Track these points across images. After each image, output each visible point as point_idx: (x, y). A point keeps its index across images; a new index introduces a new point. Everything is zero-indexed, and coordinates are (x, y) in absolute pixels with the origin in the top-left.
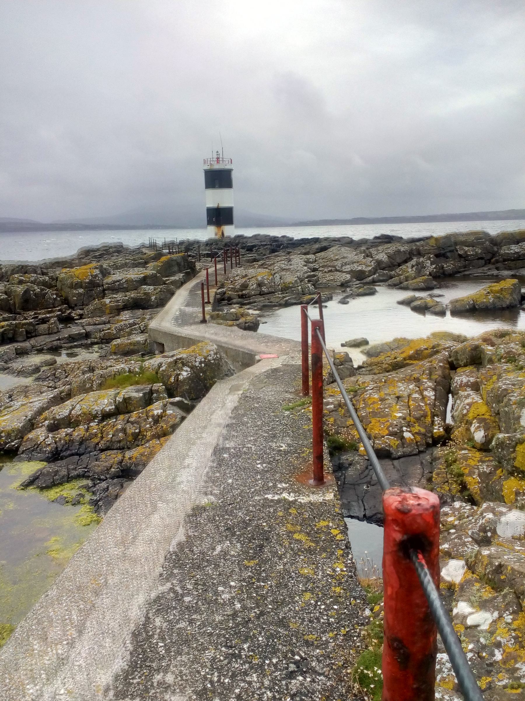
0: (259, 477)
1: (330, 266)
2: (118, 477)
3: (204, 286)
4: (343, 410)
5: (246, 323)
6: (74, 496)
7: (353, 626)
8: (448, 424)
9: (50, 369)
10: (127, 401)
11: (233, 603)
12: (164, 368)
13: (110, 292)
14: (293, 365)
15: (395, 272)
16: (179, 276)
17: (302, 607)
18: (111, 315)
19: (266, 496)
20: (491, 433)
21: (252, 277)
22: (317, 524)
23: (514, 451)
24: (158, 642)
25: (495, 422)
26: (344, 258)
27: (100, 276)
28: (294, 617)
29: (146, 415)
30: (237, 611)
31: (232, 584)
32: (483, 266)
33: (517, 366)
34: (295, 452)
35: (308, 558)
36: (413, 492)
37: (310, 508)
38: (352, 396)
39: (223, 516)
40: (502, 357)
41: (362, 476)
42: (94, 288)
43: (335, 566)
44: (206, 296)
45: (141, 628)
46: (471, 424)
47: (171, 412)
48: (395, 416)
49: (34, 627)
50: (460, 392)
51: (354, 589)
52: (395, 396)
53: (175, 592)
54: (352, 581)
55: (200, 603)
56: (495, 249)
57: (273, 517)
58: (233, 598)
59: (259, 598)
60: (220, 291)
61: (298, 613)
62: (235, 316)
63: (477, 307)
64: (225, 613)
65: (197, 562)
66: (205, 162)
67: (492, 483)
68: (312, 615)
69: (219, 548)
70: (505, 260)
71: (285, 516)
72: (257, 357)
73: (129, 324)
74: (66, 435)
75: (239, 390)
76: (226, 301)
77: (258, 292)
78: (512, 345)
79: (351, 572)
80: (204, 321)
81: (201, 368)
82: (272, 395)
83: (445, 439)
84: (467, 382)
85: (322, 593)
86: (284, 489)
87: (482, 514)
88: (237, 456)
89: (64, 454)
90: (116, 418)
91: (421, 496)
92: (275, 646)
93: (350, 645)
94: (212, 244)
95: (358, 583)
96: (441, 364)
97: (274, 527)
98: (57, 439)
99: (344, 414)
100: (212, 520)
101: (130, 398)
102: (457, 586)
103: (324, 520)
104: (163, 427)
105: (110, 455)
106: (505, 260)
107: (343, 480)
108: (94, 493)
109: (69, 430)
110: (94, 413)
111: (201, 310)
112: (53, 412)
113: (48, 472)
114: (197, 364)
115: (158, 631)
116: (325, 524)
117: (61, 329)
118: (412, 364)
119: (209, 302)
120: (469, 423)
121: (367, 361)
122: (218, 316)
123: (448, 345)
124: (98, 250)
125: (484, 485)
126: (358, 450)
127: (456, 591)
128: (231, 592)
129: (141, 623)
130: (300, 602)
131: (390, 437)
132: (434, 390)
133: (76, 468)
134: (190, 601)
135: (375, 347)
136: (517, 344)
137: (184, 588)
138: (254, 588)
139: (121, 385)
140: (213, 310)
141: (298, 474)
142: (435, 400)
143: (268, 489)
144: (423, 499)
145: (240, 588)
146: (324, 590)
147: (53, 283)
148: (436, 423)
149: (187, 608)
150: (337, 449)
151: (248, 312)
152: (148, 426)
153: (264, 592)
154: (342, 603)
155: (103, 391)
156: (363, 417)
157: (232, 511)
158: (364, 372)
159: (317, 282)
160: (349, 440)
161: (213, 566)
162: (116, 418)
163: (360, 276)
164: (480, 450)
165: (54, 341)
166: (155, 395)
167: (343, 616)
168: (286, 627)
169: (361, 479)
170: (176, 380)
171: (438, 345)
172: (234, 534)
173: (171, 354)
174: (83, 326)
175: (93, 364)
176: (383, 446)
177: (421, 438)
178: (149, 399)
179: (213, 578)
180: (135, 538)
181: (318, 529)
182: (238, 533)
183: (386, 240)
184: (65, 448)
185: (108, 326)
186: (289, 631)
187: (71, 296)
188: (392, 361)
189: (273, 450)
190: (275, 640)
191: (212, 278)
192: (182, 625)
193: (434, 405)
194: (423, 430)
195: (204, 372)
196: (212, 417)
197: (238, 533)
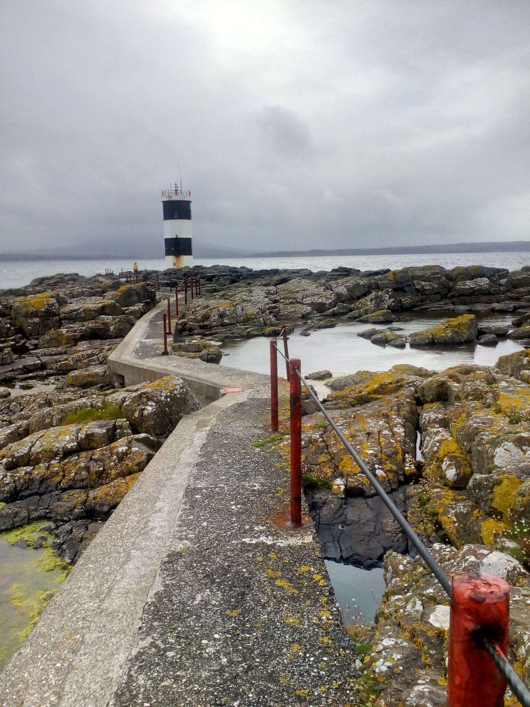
0: (234, 519)
1: (291, 298)
2: (82, 518)
3: (166, 316)
4: (314, 447)
5: (208, 355)
6: (36, 539)
7: (345, 678)
8: (419, 461)
9: (4, 402)
10: (90, 437)
11: (219, 657)
12: (128, 403)
13: (67, 321)
14: (259, 399)
15: (355, 305)
16: (138, 307)
17: (290, 660)
18: (68, 345)
19: (243, 540)
20: (462, 471)
21: (214, 308)
22: (298, 569)
23: (492, 492)
24: (143, 703)
25: (466, 460)
26: (304, 290)
27: (57, 305)
28: (284, 671)
29: (111, 453)
30: (223, 666)
31: (216, 636)
32: (439, 301)
33: (484, 404)
34: (269, 492)
35: (292, 607)
36: (482, 578)
37: (290, 552)
38: (322, 432)
39: (200, 562)
40: (468, 395)
41: (337, 516)
42: (50, 318)
43: (321, 614)
44: (167, 326)
45: (124, 687)
46: (442, 461)
47: (137, 449)
48: (367, 453)
49: (7, 690)
50: (428, 428)
51: (342, 639)
52: (365, 432)
53: (156, 647)
54: (339, 630)
55: (183, 658)
56: (451, 284)
57: (253, 562)
58: (218, 651)
59: (245, 651)
60: (181, 321)
61: (287, 667)
62: (197, 347)
63: (436, 341)
64: (212, 668)
65: (177, 613)
66: (163, 194)
67: (470, 523)
68: (302, 668)
69: (199, 598)
70: (460, 295)
71: (265, 561)
72: (222, 391)
73: (87, 355)
74: (26, 474)
75: (206, 426)
76: (187, 332)
77: (220, 324)
78: (478, 382)
79: (337, 620)
80: (165, 353)
81: (167, 402)
82: (240, 431)
83: (417, 476)
84: (435, 419)
85: (310, 644)
86: (261, 532)
87: (464, 557)
88: (210, 496)
89: (24, 493)
90: (78, 456)
91: (491, 582)
92: (266, 702)
93: (344, 700)
94: (171, 273)
95: (345, 632)
96: (408, 400)
97: (255, 573)
98: (16, 478)
99: (315, 451)
100: (189, 567)
101: (92, 434)
102: (446, 634)
103: (305, 565)
104: (128, 465)
105: (72, 495)
106: (460, 295)
107: (317, 520)
108: (57, 536)
109: (29, 469)
110: (55, 450)
111: (163, 341)
112: (12, 449)
113: (8, 513)
114: (163, 398)
115: (142, 690)
116: (307, 570)
117: (15, 359)
118: (377, 399)
119: (170, 333)
120: (440, 460)
121: (332, 394)
122: (180, 348)
123: (411, 380)
124: (52, 278)
125: (462, 525)
126: (331, 489)
127: (446, 639)
128: (215, 646)
129: (124, 681)
130: (288, 655)
131: (362, 475)
132: (404, 426)
133: (37, 508)
134: (173, 656)
135: (339, 380)
136: (482, 382)
137: (166, 642)
138: (239, 640)
139: (83, 420)
140: (175, 341)
141: (274, 515)
142: (405, 436)
143: (245, 532)
144: (494, 586)
145: (224, 641)
146: (312, 641)
147: (7, 312)
148: (407, 460)
149: (171, 663)
150: (312, 487)
151: (210, 344)
152: (112, 464)
153: (250, 644)
154: (331, 655)
155: (64, 427)
156: (335, 454)
157: (209, 557)
158: (329, 406)
159: (278, 313)
160: (322, 478)
161: (194, 617)
162: (78, 456)
163: (320, 308)
164: (452, 488)
165: (8, 372)
166: (118, 431)
167: (333, 669)
168: (276, 681)
169: (335, 519)
170: (140, 415)
171: (402, 380)
172: (213, 582)
173: (135, 388)
174: (38, 357)
175: (50, 397)
176: (356, 484)
177: (393, 476)
178: (112, 436)
179: (195, 631)
180: (110, 589)
181: (300, 575)
182: (218, 580)
183: (345, 273)
184: (24, 487)
185: (65, 357)
186: (279, 686)
187: (25, 325)
188: (359, 395)
189: (247, 490)
190: (266, 697)
191: (173, 309)
192: (167, 683)
193: (405, 442)
194: (395, 468)
195: (170, 407)
196: (180, 456)
197: (218, 580)
